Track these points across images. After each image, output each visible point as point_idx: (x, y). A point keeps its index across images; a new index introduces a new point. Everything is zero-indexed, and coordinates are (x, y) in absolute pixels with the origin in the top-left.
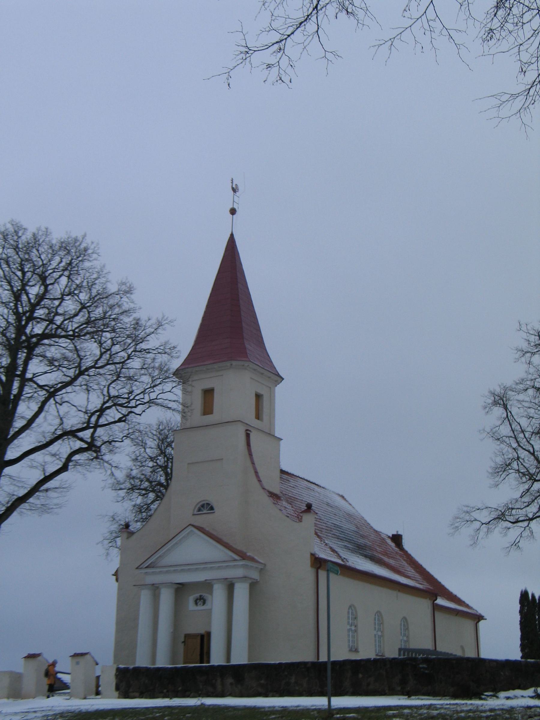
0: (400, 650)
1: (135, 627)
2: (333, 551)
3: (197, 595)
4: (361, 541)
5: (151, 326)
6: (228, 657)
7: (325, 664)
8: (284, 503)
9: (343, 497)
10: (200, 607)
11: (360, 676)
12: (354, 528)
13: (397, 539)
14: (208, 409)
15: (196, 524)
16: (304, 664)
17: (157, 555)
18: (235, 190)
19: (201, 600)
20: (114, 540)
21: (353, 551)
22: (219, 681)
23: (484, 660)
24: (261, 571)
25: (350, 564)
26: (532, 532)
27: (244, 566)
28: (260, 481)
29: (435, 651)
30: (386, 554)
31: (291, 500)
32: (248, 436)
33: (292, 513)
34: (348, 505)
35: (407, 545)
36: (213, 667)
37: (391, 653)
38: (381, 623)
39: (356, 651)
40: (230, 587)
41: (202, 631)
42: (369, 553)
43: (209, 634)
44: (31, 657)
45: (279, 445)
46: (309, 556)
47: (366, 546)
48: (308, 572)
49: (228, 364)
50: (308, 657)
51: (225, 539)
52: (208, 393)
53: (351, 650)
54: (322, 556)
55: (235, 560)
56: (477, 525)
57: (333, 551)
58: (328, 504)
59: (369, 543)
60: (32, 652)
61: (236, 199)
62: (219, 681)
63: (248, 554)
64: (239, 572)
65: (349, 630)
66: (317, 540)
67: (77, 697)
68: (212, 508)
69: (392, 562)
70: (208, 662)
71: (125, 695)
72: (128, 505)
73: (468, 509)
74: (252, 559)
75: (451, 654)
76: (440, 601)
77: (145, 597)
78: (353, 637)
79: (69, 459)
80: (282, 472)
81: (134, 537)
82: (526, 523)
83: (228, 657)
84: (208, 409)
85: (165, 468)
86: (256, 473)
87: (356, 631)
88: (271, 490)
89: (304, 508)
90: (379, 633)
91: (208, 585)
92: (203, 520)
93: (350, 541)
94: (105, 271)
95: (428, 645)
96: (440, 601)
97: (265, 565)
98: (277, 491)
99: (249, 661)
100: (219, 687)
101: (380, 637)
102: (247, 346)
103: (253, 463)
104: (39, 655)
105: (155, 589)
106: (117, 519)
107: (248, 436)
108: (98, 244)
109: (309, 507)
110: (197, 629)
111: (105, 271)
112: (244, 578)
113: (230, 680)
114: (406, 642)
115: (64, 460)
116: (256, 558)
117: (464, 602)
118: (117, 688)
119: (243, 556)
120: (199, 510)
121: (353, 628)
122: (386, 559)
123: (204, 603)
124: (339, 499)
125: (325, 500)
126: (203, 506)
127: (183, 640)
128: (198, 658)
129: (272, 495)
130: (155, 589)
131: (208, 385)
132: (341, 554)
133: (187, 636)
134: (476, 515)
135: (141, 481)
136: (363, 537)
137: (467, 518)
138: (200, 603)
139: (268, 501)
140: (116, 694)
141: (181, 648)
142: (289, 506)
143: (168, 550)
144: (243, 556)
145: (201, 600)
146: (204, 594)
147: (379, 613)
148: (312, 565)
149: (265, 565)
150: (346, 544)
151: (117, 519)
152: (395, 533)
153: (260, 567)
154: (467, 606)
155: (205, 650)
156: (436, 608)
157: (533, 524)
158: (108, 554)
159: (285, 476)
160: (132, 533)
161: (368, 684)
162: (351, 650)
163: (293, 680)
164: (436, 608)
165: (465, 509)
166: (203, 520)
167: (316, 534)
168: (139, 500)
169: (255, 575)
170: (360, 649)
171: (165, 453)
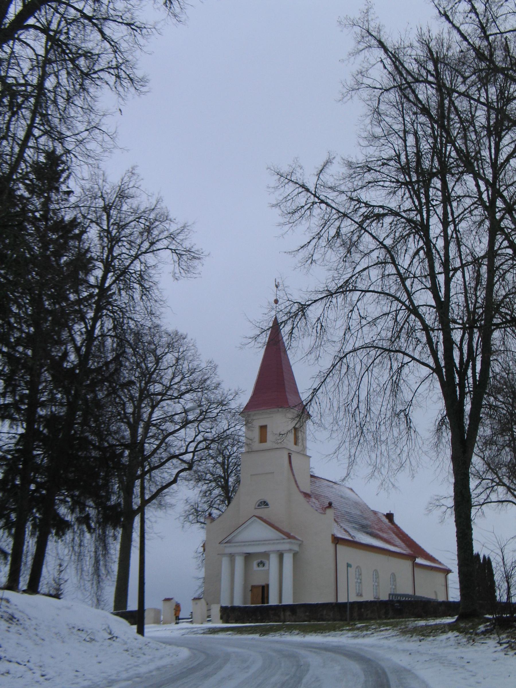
0: (390, 595)
1: (220, 580)
2: (346, 531)
3: (259, 561)
4: (365, 522)
5: (231, 394)
6: (280, 600)
7: (344, 605)
8: (313, 500)
9: (352, 489)
10: (261, 568)
11: (363, 610)
12: (359, 513)
13: (390, 516)
14: (263, 439)
15: (256, 515)
16: (331, 604)
17: (232, 535)
18: (277, 286)
19: (261, 564)
20: (187, 516)
21: (359, 530)
22: (282, 613)
23: (450, 602)
24: (300, 545)
25: (357, 540)
26: (483, 513)
27: (290, 543)
28: (298, 487)
29: (414, 596)
30: (381, 530)
31: (317, 497)
32: (290, 457)
33: (318, 506)
34: (356, 497)
35: (397, 520)
36: (271, 606)
37: (384, 597)
38: (377, 577)
39: (361, 595)
40: (281, 556)
41: (263, 583)
42: (369, 530)
43: (268, 586)
44: (167, 600)
45: (309, 461)
46: (330, 536)
47: (367, 525)
48: (330, 546)
49: (276, 410)
50: (331, 599)
51: (276, 525)
52: (263, 428)
53: (357, 595)
54: (339, 535)
55: (284, 539)
56: (444, 508)
57: (346, 531)
58: (342, 497)
59: (370, 523)
60: (167, 597)
61: (278, 293)
62: (282, 613)
63: (292, 534)
64: (287, 547)
65: (356, 582)
66: (336, 524)
67: (197, 623)
68: (267, 505)
69: (385, 535)
70: (268, 603)
71: (227, 622)
72: (197, 490)
73: (438, 498)
74: (294, 538)
75: (424, 597)
76: (419, 561)
77: (225, 562)
78: (359, 586)
79: (177, 475)
80: (312, 476)
81: (215, 522)
82: (478, 507)
83: (280, 600)
84: (263, 439)
85: (223, 464)
86: (296, 481)
87: (361, 583)
88: (305, 491)
89: (327, 504)
90: (376, 584)
91: (266, 555)
92: (263, 512)
93: (355, 523)
94: (198, 354)
95: (410, 592)
96: (419, 561)
97: (302, 541)
98: (308, 492)
99: (294, 602)
100: (282, 617)
101: (376, 586)
102: (289, 397)
103: (294, 475)
104: (172, 599)
105: (232, 557)
106: (189, 501)
107: (290, 457)
108: (195, 340)
109: (330, 504)
110: (259, 581)
111: (198, 354)
112: (290, 550)
113: (288, 613)
114: (394, 589)
115: (174, 476)
116: (297, 537)
117: (437, 560)
118: (221, 618)
119: (289, 536)
120: (259, 506)
121: (359, 581)
122: (380, 534)
123: (264, 566)
124: (349, 492)
125: (340, 493)
126: (261, 503)
127: (250, 589)
128: (260, 600)
129: (307, 495)
130: (232, 557)
131: (263, 423)
132: (351, 533)
133: (253, 587)
134: (443, 501)
135: (206, 474)
136: (365, 519)
137: (438, 504)
138: (261, 565)
139: (301, 497)
140: (221, 621)
141: (250, 594)
142: (316, 502)
143: (240, 532)
144: (289, 536)
145: (261, 564)
146: (263, 560)
147: (376, 571)
148: (333, 542)
149: (302, 541)
150: (354, 525)
151: (189, 501)
152: (388, 512)
153: (299, 542)
154: (440, 563)
155: (266, 595)
156: (416, 565)
157: (484, 507)
158: (183, 527)
159: (313, 479)
160: (213, 520)
161: (367, 615)
162: (357, 595)
163: (325, 612)
164: (416, 565)
165: (436, 498)
166: (263, 512)
167: (335, 520)
168: (205, 487)
169: (296, 548)
170: (363, 595)
171: (223, 453)
